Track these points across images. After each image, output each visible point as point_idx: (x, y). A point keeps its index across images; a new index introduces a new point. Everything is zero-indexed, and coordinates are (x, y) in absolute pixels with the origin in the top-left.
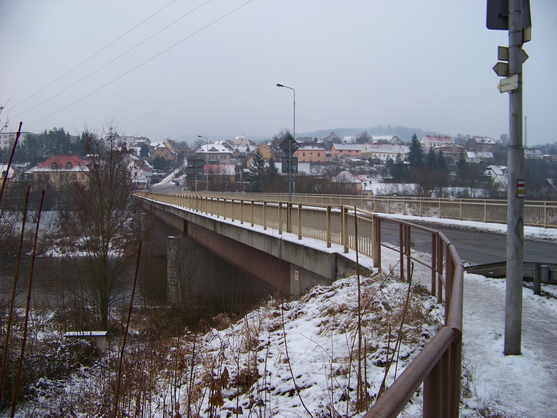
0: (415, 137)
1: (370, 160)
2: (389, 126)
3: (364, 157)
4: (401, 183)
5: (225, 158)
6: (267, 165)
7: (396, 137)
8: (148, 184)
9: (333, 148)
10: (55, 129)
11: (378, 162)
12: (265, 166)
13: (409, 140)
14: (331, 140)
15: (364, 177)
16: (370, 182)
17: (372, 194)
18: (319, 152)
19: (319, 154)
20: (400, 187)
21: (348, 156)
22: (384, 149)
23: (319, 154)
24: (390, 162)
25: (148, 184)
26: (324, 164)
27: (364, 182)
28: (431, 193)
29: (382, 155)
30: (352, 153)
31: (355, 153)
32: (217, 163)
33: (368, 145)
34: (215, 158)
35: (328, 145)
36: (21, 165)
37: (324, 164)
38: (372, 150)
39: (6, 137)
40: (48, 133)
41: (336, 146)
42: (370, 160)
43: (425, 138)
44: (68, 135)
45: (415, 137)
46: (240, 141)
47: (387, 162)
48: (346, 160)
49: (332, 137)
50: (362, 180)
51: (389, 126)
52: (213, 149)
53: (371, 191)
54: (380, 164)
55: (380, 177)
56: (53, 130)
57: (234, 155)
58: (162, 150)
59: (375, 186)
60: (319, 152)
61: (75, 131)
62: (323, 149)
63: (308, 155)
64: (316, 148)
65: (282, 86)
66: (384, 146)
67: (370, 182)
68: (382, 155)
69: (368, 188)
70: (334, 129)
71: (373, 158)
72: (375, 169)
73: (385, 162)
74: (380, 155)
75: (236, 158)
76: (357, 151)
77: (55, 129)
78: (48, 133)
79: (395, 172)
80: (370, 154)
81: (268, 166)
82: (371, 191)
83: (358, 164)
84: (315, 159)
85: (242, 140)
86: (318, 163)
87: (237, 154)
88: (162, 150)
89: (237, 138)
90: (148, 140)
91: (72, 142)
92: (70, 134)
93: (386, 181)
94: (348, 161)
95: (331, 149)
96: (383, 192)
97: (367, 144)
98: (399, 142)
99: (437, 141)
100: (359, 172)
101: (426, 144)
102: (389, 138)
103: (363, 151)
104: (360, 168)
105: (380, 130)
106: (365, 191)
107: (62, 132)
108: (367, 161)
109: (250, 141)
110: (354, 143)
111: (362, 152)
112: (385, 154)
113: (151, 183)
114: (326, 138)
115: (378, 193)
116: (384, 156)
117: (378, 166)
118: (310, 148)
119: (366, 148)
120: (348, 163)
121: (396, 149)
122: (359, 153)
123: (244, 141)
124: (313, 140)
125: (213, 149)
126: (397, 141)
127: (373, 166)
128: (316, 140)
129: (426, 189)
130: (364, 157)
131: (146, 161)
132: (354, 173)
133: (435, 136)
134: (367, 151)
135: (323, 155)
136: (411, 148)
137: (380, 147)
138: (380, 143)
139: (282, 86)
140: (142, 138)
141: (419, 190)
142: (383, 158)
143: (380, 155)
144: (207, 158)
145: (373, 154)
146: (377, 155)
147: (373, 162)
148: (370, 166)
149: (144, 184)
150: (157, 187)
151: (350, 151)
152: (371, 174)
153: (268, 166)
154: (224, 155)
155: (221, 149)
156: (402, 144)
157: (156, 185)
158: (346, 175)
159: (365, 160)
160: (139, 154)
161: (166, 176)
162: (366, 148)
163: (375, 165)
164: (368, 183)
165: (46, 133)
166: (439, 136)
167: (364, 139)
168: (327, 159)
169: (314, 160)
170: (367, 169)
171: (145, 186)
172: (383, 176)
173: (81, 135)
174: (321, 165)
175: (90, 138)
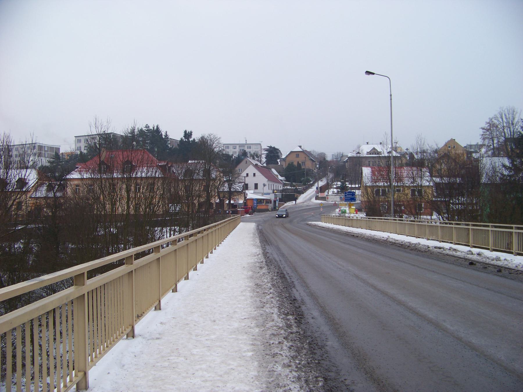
8: (275, 201)
10: (147, 126)
25: (275, 201)
56: (144, 129)
58: (298, 156)
77: (147, 126)
88: (298, 156)
107: (157, 131)
113: (281, 200)
131: (274, 170)
149: (268, 201)
161: (305, 190)
165: (133, 131)
171: (271, 206)
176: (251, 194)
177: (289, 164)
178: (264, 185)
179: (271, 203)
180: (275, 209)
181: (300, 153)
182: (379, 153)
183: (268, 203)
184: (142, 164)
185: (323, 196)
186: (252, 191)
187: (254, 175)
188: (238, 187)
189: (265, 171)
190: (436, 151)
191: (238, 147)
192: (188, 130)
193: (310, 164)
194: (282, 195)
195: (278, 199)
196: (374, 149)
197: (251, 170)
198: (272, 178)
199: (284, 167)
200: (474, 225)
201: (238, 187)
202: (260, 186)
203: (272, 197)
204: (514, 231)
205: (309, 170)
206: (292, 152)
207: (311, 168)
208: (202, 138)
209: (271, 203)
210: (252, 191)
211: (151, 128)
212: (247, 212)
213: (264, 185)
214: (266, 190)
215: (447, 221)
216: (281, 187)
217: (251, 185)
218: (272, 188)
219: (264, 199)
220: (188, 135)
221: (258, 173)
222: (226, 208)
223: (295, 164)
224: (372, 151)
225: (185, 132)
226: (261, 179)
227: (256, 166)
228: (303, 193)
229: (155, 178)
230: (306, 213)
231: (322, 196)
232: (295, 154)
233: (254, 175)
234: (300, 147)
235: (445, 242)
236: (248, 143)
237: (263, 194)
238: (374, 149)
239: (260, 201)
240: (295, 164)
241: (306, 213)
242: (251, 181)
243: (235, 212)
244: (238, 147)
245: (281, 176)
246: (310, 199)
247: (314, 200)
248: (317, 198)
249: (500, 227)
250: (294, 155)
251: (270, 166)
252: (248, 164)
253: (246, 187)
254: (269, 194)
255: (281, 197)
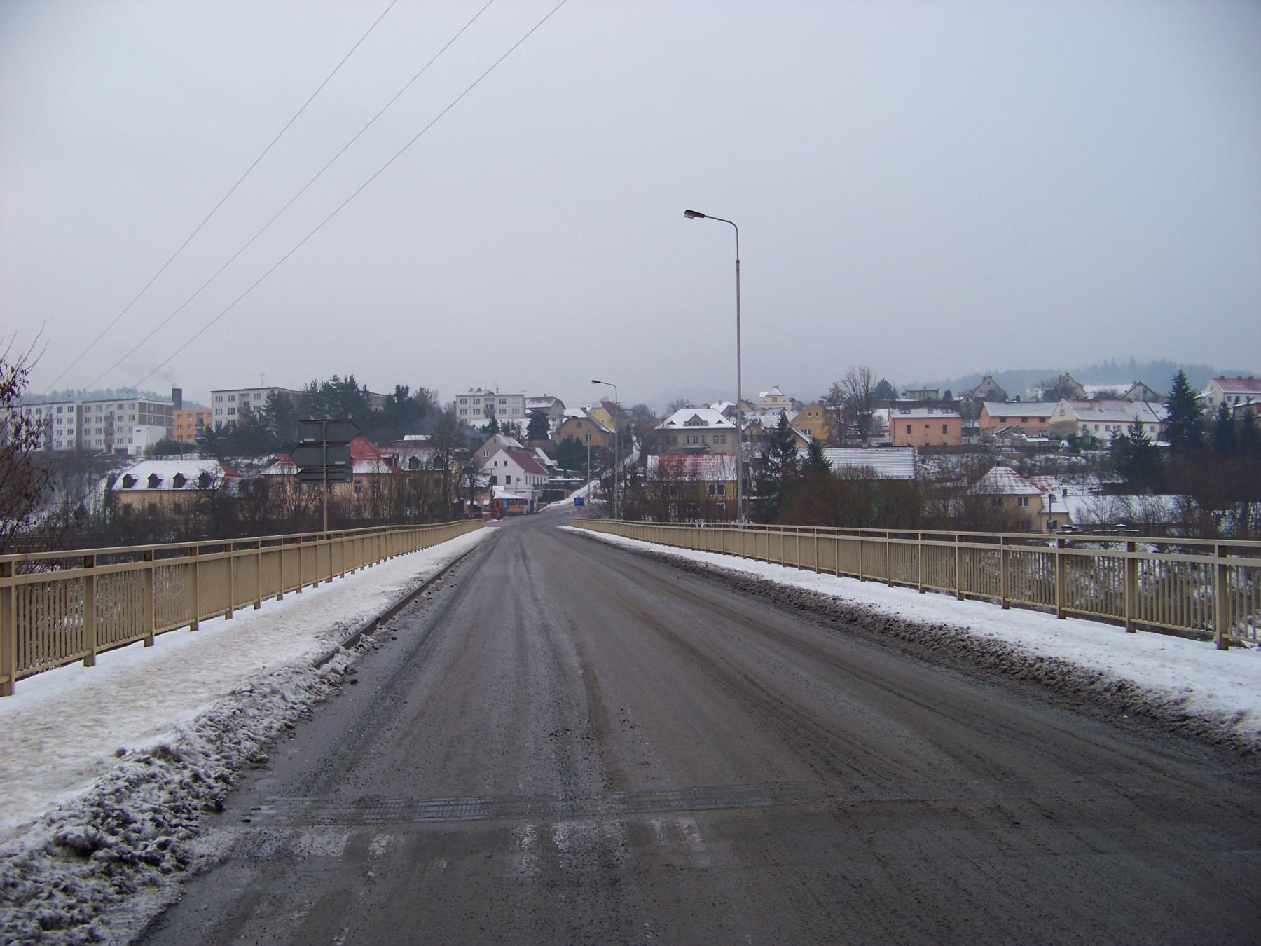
0: (1180, 381)
1: (1071, 439)
2: (1132, 361)
3: (1057, 432)
4: (1137, 494)
5: (723, 442)
6: (803, 453)
7: (1140, 384)
8: (532, 502)
9: (983, 413)
10: (335, 378)
11: (1093, 443)
12: (798, 457)
13: (1166, 389)
14: (982, 395)
15: (1051, 480)
16: (1065, 492)
17: (1069, 521)
18: (945, 422)
19: (945, 427)
20: (1137, 504)
21: (1017, 430)
22: (1106, 412)
23: (945, 427)
24: (1120, 443)
25: (532, 502)
26: (957, 450)
27: (1047, 494)
28: (1219, 517)
29: (1102, 426)
30: (1030, 424)
31: (1037, 424)
32: (698, 452)
33: (1066, 404)
34: (700, 440)
35: (969, 407)
36: (256, 461)
37: (957, 450)
38: (1077, 415)
39: (232, 399)
40: (319, 388)
41: (992, 409)
42: (1071, 439)
43: (1212, 383)
44: (365, 392)
45: (1180, 381)
46: (769, 401)
47: (1113, 442)
48: (1013, 440)
49: (986, 388)
50: (1043, 489)
51: (1132, 361)
52: (696, 420)
53: (1067, 514)
54: (1097, 448)
55: (1093, 480)
56: (331, 383)
57: (748, 433)
58: (579, 425)
59: (1075, 502)
60: (945, 422)
61: (379, 382)
62: (955, 415)
63: (918, 430)
64: (937, 413)
65: (702, 216)
66: (1106, 404)
67: (1065, 492)
68: (1102, 426)
69: (1057, 508)
70: (993, 371)
71: (1080, 434)
72: (1084, 461)
73: (1109, 445)
74: (1097, 427)
75: (752, 438)
76: (1042, 419)
77: (335, 378)
78: (319, 388)
79: (1131, 466)
80: (1072, 424)
81: (806, 456)
82: (1067, 514)
83: (1041, 448)
84: (935, 437)
85: (774, 399)
86: (944, 449)
87: (755, 432)
88: (579, 425)
89: (763, 394)
90: (559, 402)
91: (373, 408)
92: (368, 389)
93: (1108, 489)
94: (1017, 443)
95: (978, 417)
96: (1093, 518)
97: (1063, 401)
98: (1149, 394)
99: (1243, 391)
100: (1041, 468)
101: (1210, 394)
102: (1122, 389)
103: (1056, 419)
104: (1047, 459)
105: (1109, 371)
106: (1050, 514)
107: (352, 384)
108: (1065, 443)
109: (792, 400)
110: (1038, 401)
111: (1052, 420)
112: (1105, 425)
113: (540, 500)
114: (973, 391)
115: (1081, 519)
116: (1107, 428)
117: (1090, 453)
118: (922, 413)
119: (1062, 412)
120: (1017, 449)
121: (1138, 410)
122: (1046, 425)
123: (780, 401)
124: (941, 395)
125: (696, 420)
126: (1145, 392)
127: (1077, 454)
128: (948, 394)
129: (1207, 505)
130: (1059, 432)
131: (539, 451)
132: (1025, 472)
133: (1239, 378)
134: (1066, 418)
135: (955, 428)
136: (1170, 409)
137: (1097, 407)
138: (1102, 397)
139: (702, 216)
140: (546, 399)
141: (1186, 511)
142: (1103, 434)
143: (1097, 427)
144: (681, 440)
145: (1080, 424)
146: (1091, 426)
147: (1077, 444)
148: (1065, 454)
149: (523, 502)
150: (555, 510)
151: (1024, 419)
152: (1073, 473)
153: (806, 456)
154: (720, 433)
155: (713, 417)
156: (1156, 399)
157: (554, 504)
158: (1003, 479)
159: (1060, 438)
160: (525, 433)
161: (583, 483)
162: (1062, 412)
163: (1082, 452)
164: (1058, 494)
165: (314, 388)
166: (1251, 379)
167: (1061, 390)
168: (964, 441)
169: (934, 442)
170: (1063, 460)
171: (527, 507)
172: (1101, 477)
173: (393, 392)
174: (951, 453)
175: (280, 395)
176: (500, 492)
178: (518, 480)
180: (531, 512)
182: (705, 423)
184: (362, 456)
186: (502, 488)
188: (483, 481)
189: (522, 457)
191: (482, 400)
192: (403, 385)
196: (696, 416)
197: (501, 456)
198: (530, 465)
199: (558, 443)
201: (483, 481)
202: (513, 480)
208: (422, 393)
210: (502, 488)
211: (342, 381)
212: (494, 517)
213: (518, 480)
214: (522, 485)
215: (751, 524)
216: (545, 480)
217: (501, 479)
220: (402, 392)
221: (511, 462)
222: (466, 510)
225: (398, 387)
226: (516, 470)
227: (509, 450)
229: (379, 474)
235: (978, 598)
238: (696, 416)
239: (511, 502)
242: (501, 473)
243: (479, 516)
244: (482, 400)
245: (551, 459)
251: (535, 442)
252: (498, 446)
253: (494, 480)
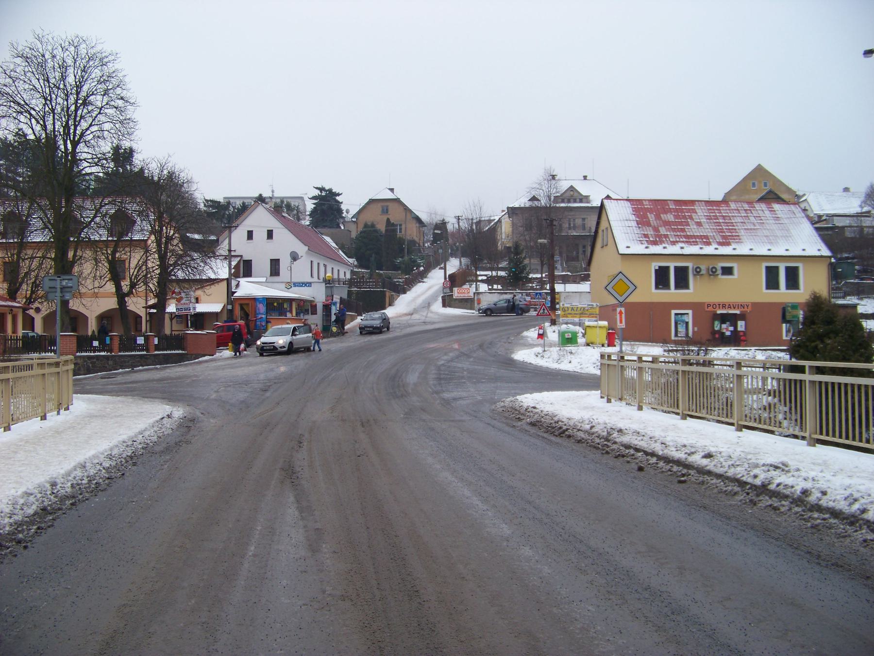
8: (327, 308)
88: (385, 211)
131: (328, 239)
177: (366, 226)
178: (294, 257)
179: (314, 312)
181: (390, 204)
183: (306, 312)
185: (466, 296)
187: (270, 234)
190: (110, 457)
193: (415, 229)
194: (350, 293)
195: (337, 299)
199: (354, 235)
200: (820, 371)
203: (317, 294)
204: (807, 377)
205: (412, 242)
206: (372, 201)
207: (417, 239)
209: (314, 312)
214: (302, 270)
217: (261, 266)
218: (322, 275)
219: (290, 301)
223: (382, 227)
224: (567, 194)
228: (404, 292)
230: (432, 345)
231: (461, 296)
232: (380, 204)
233: (270, 234)
234: (392, 190)
236: (276, 195)
237: (290, 285)
240: (382, 227)
241: (432, 345)
246: (428, 305)
247: (438, 307)
248: (448, 301)
249: (834, 371)
250: (378, 207)
254: (308, 284)
255: (345, 296)
